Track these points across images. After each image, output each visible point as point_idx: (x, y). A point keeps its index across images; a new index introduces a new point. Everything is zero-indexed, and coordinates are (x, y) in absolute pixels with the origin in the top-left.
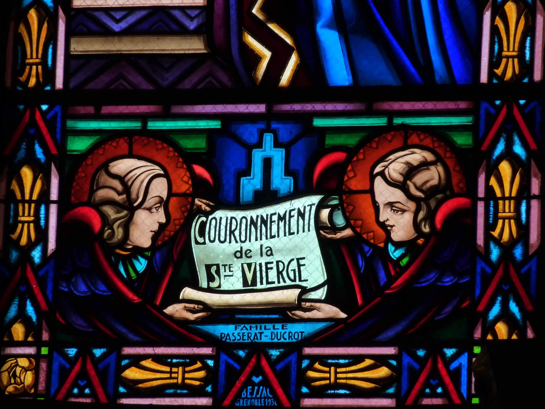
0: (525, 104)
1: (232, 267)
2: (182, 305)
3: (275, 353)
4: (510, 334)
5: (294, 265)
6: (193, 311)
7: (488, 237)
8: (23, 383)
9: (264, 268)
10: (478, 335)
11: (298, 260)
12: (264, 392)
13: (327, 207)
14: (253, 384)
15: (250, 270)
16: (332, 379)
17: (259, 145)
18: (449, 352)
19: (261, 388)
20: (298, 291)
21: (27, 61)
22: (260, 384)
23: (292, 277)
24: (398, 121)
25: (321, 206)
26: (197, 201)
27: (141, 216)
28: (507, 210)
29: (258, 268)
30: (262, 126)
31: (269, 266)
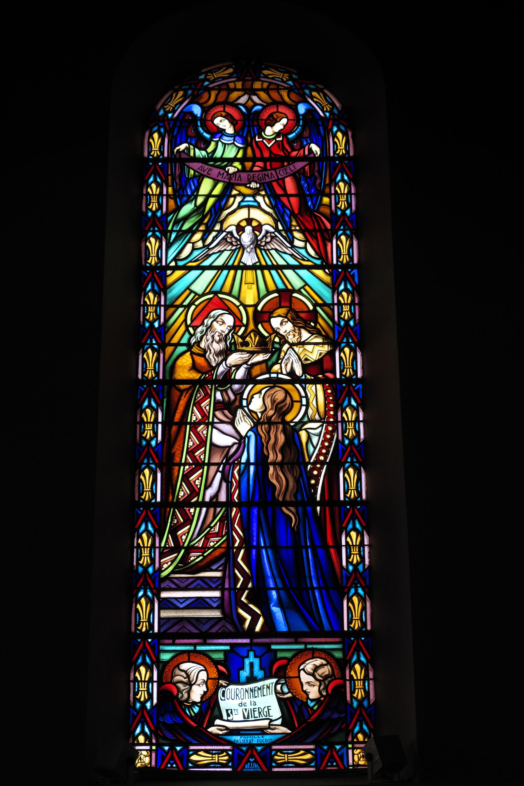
19: (254, 764)
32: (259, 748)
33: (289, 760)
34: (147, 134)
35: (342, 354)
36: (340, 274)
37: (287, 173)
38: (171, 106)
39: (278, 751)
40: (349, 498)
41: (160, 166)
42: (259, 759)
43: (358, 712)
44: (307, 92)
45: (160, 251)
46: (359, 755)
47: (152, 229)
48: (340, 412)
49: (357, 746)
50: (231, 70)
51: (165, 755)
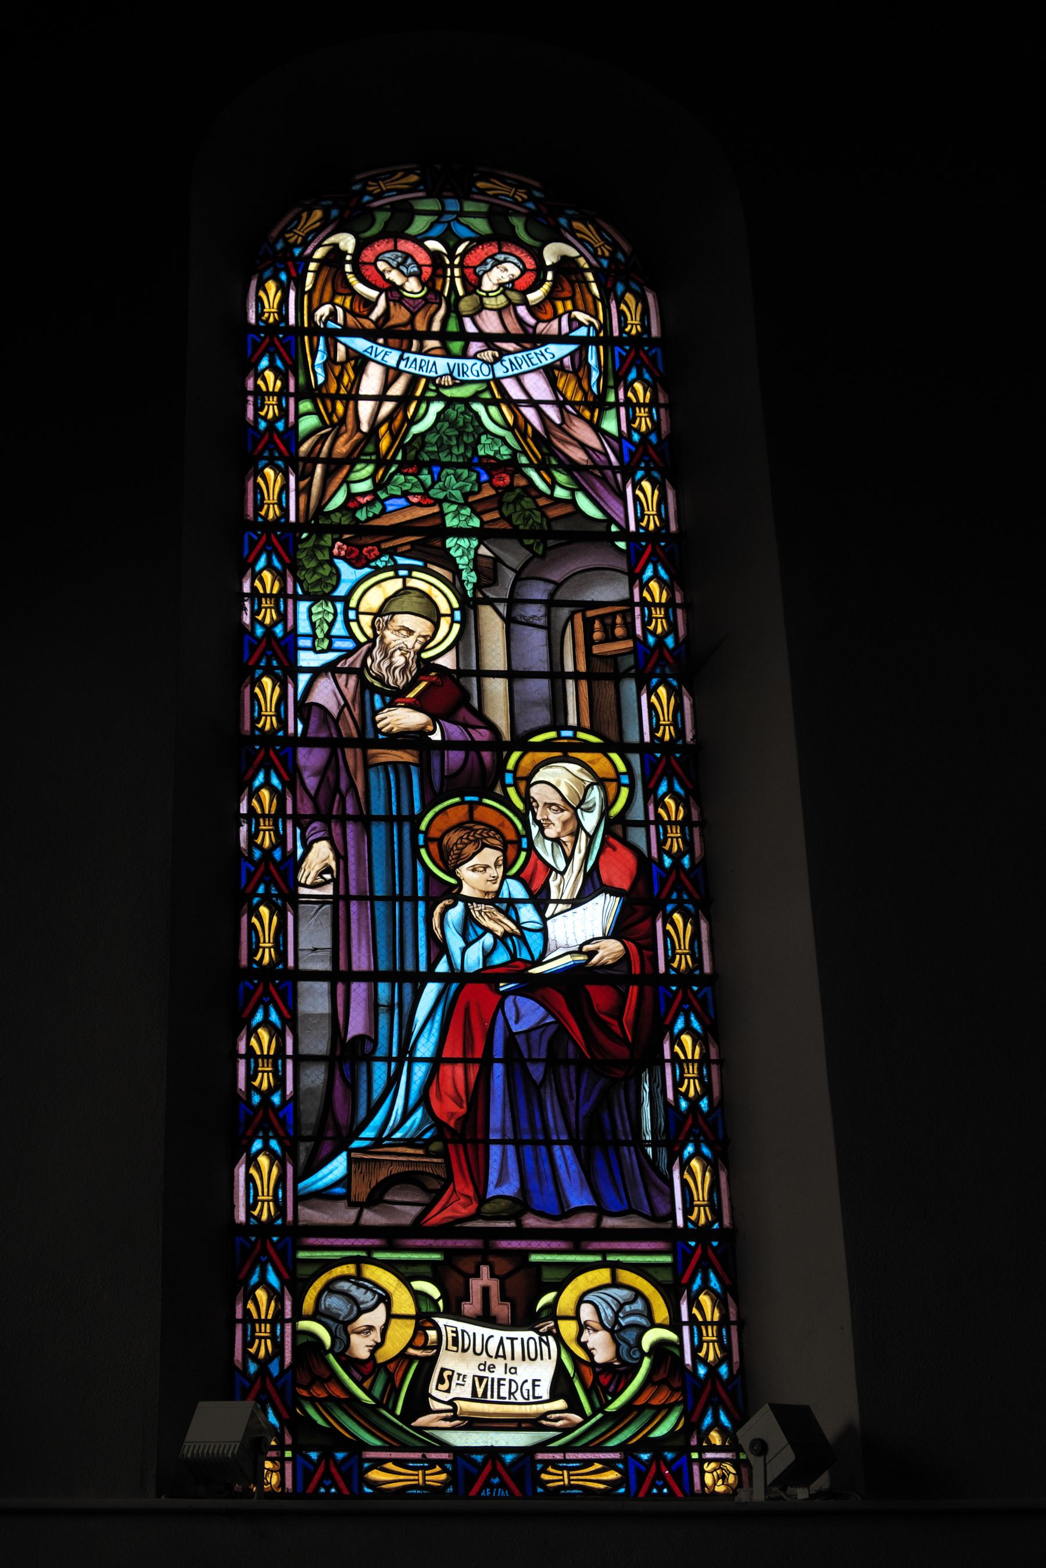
1: (539, 1386)
7: (246, 1354)
8: (270, 1483)
9: (496, 1384)
10: (694, 1442)
12: (503, 1492)
14: (492, 1486)
15: (480, 1384)
19: (500, 1490)
22: (498, 1486)
24: (610, 1258)
29: (490, 1383)
30: (479, 1259)
31: (502, 1382)
32: (509, 1458)
33: (572, 1482)
34: (254, 284)
35: (653, 699)
36: (675, 997)
37: (533, 364)
38: (299, 235)
39: (547, 1463)
40: (695, 1223)
41: (280, 340)
42: (508, 1479)
43: (709, 1388)
44: (563, 221)
45: (284, 496)
46: (715, 1473)
47: (266, 454)
48: (660, 920)
49: (709, 1455)
50: (414, 178)
51: (312, 1468)
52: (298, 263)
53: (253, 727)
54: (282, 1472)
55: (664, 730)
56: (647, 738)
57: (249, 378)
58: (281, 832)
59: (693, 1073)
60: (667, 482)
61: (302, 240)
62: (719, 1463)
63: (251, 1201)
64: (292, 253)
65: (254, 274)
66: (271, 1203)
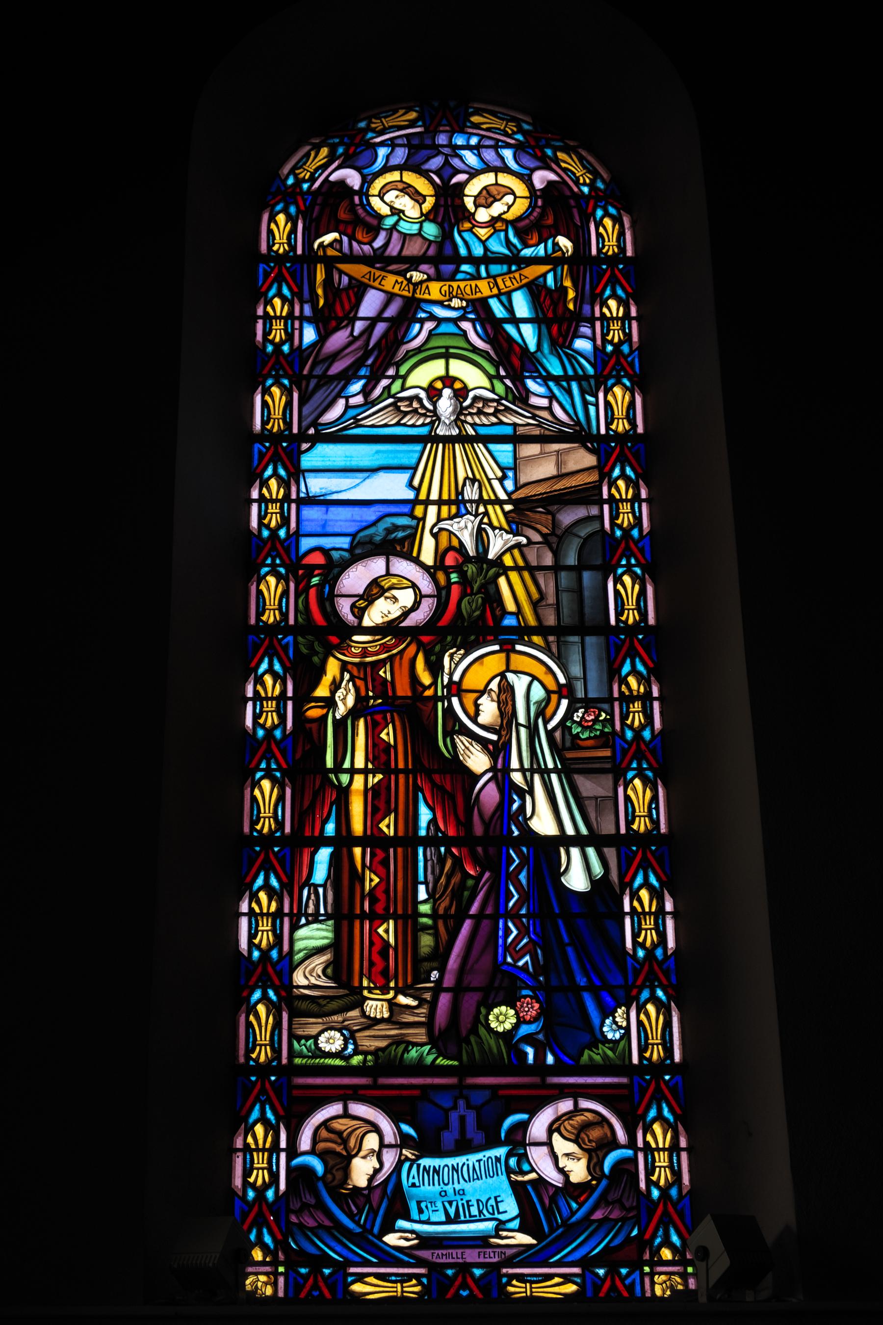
0: (670, 1080)
2: (398, 1235)
3: (478, 1272)
4: (674, 1257)
5: (492, 1202)
6: (407, 1239)
7: (649, 1182)
10: (647, 1256)
11: (496, 1198)
13: (514, 1155)
16: (529, 1293)
17: (455, 1107)
18: (624, 1271)
20: (494, 1223)
21: (257, 1042)
23: (491, 1211)
25: (509, 1155)
26: (404, 1152)
27: (357, 1162)
28: (662, 1160)
34: (266, 217)
35: (643, 1017)
36: (603, 275)
38: (308, 171)
40: (650, 1059)
50: (413, 115)
51: (302, 1281)
52: (305, 197)
53: (248, 1058)
54: (275, 1285)
55: (660, 1171)
56: (623, 831)
57: (257, 395)
58: (286, 514)
59: (650, 924)
60: (659, 782)
61: (310, 176)
62: (669, 1276)
63: (258, 711)
64: (301, 188)
65: (266, 208)
66: (271, 819)
